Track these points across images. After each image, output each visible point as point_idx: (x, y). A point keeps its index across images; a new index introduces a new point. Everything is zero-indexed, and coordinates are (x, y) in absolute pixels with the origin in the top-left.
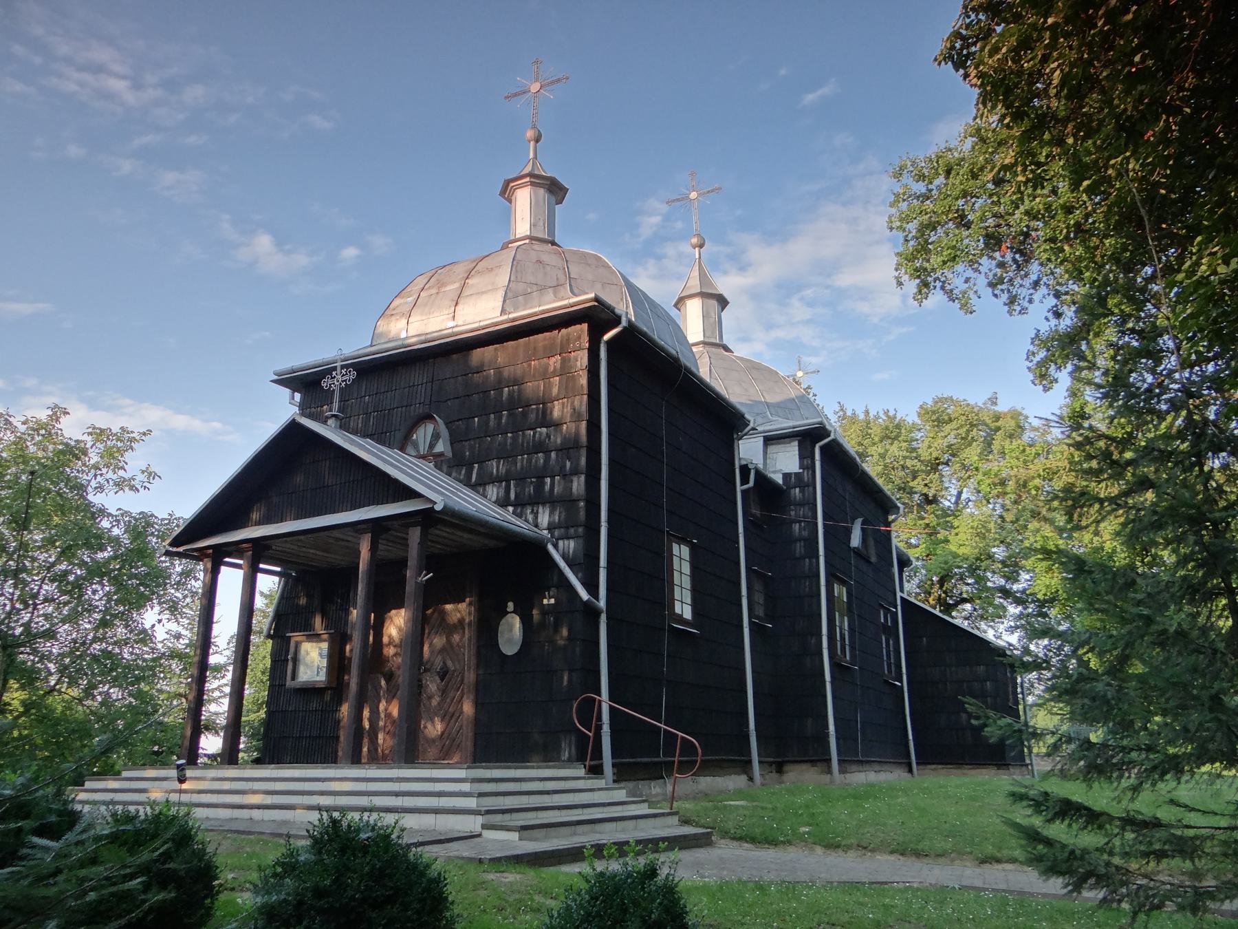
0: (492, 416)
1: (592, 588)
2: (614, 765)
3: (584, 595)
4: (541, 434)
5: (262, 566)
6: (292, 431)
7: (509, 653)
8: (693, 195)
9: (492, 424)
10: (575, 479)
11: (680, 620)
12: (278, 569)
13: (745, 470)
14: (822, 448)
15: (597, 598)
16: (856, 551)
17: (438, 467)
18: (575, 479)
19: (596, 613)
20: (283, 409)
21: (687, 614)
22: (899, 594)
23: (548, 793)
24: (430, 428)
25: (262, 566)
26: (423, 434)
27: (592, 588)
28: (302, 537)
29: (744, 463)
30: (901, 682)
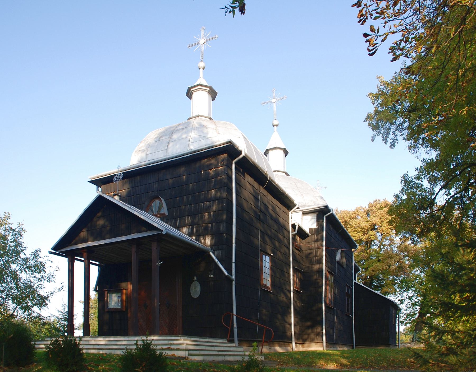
0: (185, 197)
1: (230, 271)
2: (238, 340)
3: (226, 274)
4: (206, 204)
5: (91, 261)
6: (100, 199)
7: (195, 297)
8: (274, 100)
9: (185, 200)
10: (222, 224)
11: (265, 286)
12: (98, 263)
13: (294, 226)
14: (326, 217)
15: (231, 275)
16: (338, 262)
17: (162, 219)
18: (222, 224)
19: (231, 281)
20: (93, 193)
21: (268, 284)
22: (354, 281)
23: (213, 346)
24: (158, 202)
25: (91, 261)
26: (156, 204)
27: (230, 271)
28: (107, 247)
29: (293, 223)
30: (352, 316)
